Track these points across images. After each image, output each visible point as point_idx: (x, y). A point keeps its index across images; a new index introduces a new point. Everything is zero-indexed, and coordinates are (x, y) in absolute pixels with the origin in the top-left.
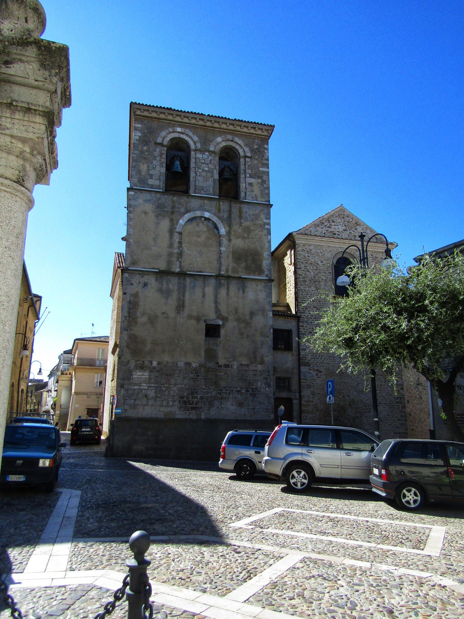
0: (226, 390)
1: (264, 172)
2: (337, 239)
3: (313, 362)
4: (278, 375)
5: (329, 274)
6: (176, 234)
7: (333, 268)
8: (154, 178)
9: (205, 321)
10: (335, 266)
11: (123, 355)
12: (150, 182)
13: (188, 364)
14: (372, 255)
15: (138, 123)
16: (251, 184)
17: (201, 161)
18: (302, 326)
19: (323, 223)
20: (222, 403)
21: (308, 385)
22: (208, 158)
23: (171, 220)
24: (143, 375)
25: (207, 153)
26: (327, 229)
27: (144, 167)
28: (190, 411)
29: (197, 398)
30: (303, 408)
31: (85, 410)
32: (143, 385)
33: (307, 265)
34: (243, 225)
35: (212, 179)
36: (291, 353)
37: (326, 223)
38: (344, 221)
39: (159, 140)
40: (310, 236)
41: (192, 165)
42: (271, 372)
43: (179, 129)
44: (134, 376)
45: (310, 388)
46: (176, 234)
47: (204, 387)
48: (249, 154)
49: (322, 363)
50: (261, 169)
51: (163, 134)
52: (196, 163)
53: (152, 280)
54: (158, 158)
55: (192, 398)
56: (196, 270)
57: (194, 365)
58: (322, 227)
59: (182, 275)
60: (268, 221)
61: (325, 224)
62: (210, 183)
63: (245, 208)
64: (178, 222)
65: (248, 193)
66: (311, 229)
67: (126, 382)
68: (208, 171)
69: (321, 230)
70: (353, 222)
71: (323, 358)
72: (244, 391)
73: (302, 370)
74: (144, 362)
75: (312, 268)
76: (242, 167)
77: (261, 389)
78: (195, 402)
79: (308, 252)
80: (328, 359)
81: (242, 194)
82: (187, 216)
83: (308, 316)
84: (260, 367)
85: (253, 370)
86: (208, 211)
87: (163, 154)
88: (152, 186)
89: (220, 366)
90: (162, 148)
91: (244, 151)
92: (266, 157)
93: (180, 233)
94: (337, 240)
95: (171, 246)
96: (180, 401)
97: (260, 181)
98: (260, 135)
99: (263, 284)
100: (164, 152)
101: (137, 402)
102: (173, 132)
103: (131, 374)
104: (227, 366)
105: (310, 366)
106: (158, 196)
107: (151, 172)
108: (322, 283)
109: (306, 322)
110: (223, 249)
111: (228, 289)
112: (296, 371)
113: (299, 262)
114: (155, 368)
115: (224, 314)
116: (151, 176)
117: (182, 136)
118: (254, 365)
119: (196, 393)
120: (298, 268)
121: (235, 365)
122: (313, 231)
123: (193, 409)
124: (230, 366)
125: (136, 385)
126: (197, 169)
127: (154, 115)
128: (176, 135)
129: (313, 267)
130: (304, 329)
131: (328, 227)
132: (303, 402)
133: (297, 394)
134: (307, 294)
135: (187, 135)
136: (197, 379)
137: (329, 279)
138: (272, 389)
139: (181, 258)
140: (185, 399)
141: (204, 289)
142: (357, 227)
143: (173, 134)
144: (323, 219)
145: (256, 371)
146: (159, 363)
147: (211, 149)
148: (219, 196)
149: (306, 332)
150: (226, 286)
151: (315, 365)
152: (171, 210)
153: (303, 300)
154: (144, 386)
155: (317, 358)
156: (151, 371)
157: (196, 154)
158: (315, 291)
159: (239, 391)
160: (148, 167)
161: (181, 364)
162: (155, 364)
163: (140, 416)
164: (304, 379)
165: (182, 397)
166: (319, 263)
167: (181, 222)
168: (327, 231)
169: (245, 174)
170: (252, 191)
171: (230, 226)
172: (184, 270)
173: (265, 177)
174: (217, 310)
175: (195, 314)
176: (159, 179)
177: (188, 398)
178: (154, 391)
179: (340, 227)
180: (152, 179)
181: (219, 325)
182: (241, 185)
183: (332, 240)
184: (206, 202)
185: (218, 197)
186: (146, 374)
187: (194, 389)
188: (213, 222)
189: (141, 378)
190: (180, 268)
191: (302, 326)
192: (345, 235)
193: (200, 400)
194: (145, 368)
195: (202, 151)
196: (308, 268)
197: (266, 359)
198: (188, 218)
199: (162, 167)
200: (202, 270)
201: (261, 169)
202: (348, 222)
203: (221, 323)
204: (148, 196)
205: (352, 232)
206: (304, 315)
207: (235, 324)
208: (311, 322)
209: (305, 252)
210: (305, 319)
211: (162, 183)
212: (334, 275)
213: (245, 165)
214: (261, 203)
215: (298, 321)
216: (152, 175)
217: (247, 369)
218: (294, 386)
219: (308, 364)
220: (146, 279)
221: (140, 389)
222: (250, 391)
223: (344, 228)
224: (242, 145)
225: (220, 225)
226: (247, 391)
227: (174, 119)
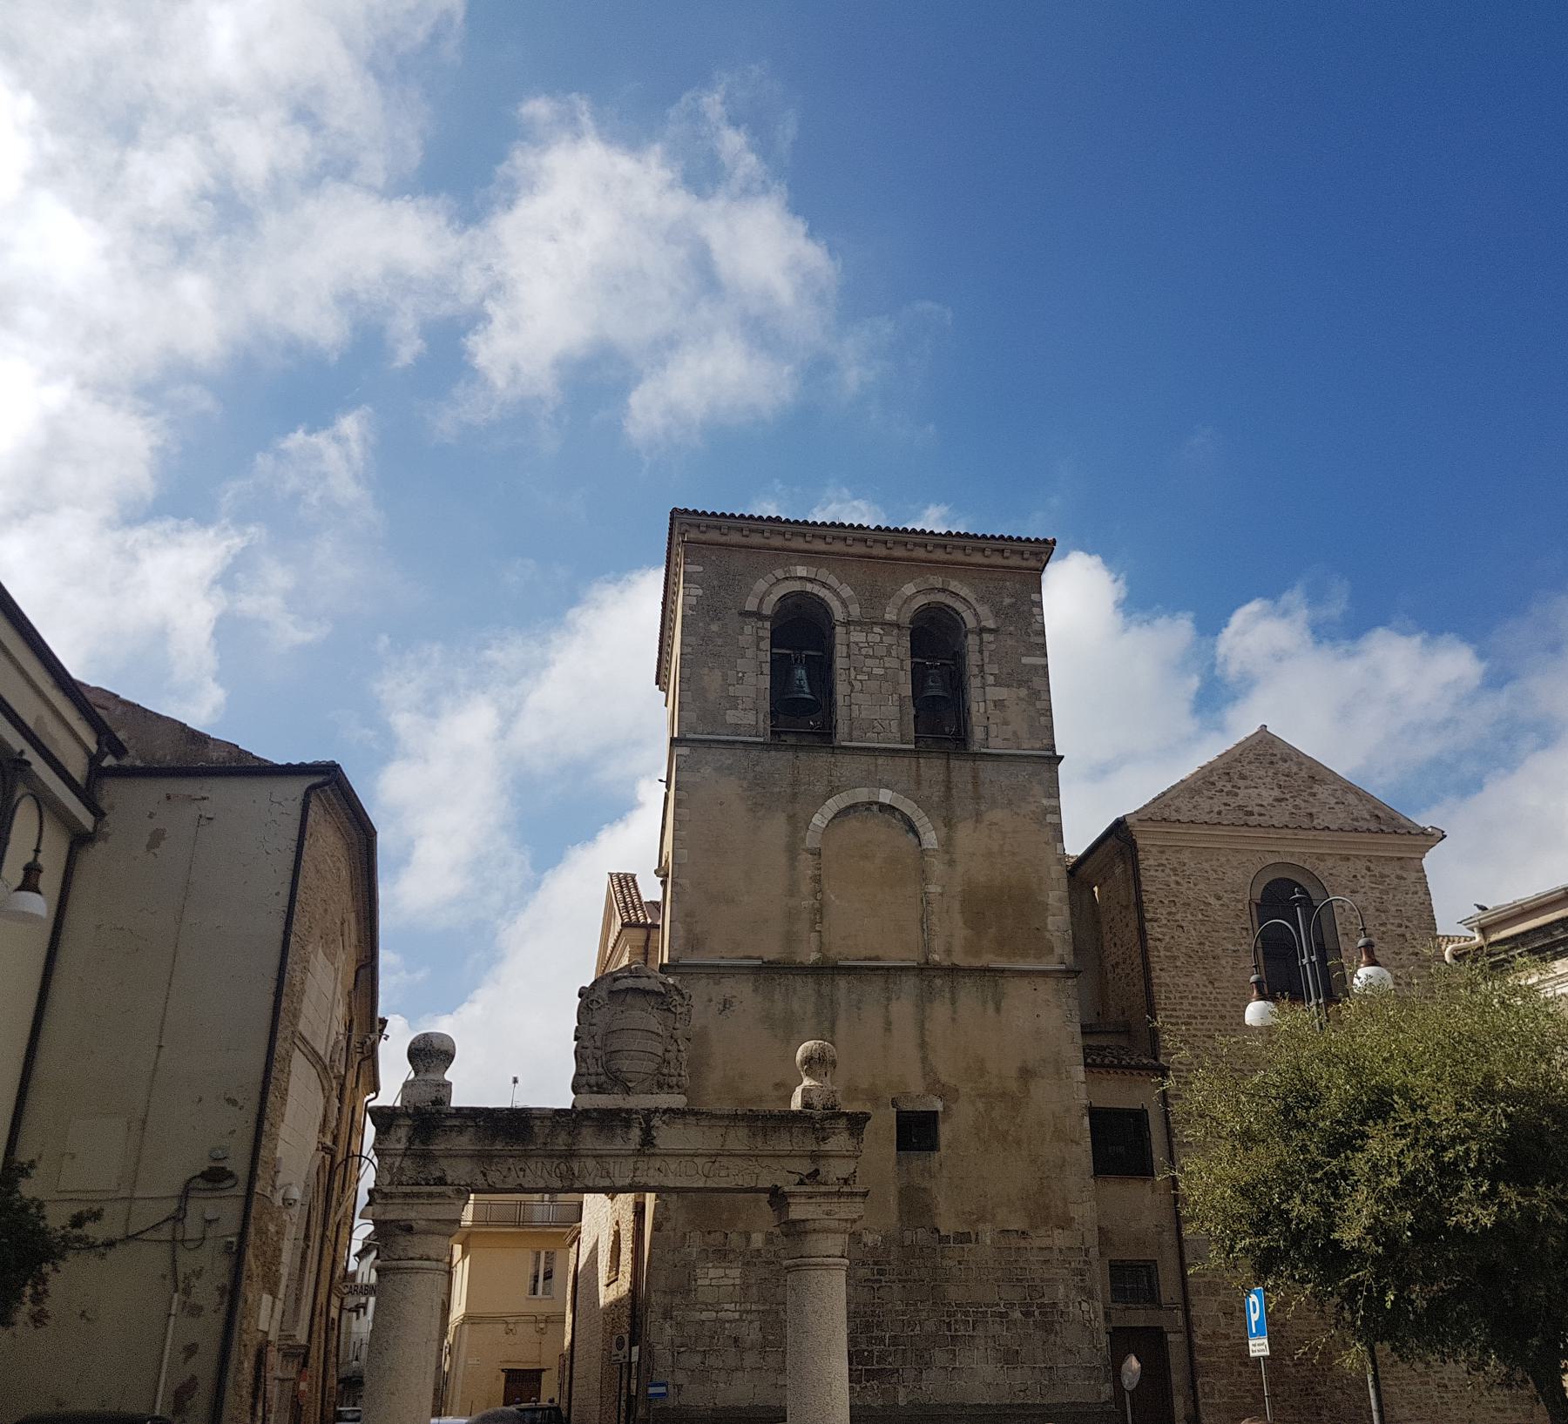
0: (966, 1314)
1: (1035, 668)
2: (1259, 829)
5: (1245, 933)
6: (804, 856)
7: (1254, 913)
8: (740, 707)
9: (894, 1103)
11: (668, 1219)
12: (731, 717)
16: (999, 704)
17: (864, 651)
19: (1213, 784)
23: (792, 818)
25: (877, 629)
27: (712, 680)
29: (882, 1340)
31: (497, 1378)
32: (726, 1306)
33: (1174, 910)
36: (1149, 1184)
37: (1222, 783)
39: (751, 605)
40: (1178, 825)
41: (840, 663)
42: (1094, 1252)
43: (801, 571)
45: (1216, 1293)
46: (804, 856)
48: (990, 624)
50: (1025, 660)
51: (761, 585)
52: (849, 656)
54: (750, 653)
55: (869, 1343)
56: (864, 953)
57: (869, 1239)
58: (1210, 794)
59: (826, 970)
60: (1053, 802)
61: (1219, 785)
62: (891, 709)
63: (988, 770)
66: (1177, 802)
67: (677, 1300)
68: (884, 678)
69: (1206, 806)
70: (1303, 774)
75: (1190, 917)
76: (973, 659)
79: (1174, 870)
81: (978, 733)
82: (834, 804)
84: (1060, 1239)
87: (762, 638)
91: (976, 614)
92: (1037, 627)
93: (817, 853)
94: (1260, 833)
95: (792, 891)
97: (1023, 692)
98: (1016, 568)
99: (1051, 983)
101: (712, 1361)
102: (787, 578)
104: (963, 1238)
108: (1223, 962)
110: (934, 889)
111: (953, 1002)
112: (1168, 1238)
116: (733, 702)
117: (809, 587)
118: (1042, 1232)
119: (879, 1324)
120: (1151, 920)
122: (1184, 809)
124: (973, 1237)
125: (707, 1306)
127: (735, 538)
128: (796, 586)
129: (1192, 914)
131: (1228, 793)
132: (1198, 1341)
133: (1180, 1313)
134: (1181, 998)
135: (824, 585)
137: (1245, 947)
138: (1099, 1306)
141: (886, 1007)
142: (1316, 788)
144: (1211, 771)
147: (887, 617)
150: (948, 995)
152: (789, 790)
153: (1171, 1016)
154: (730, 1311)
157: (848, 633)
158: (1205, 986)
159: (1001, 1315)
160: (725, 677)
166: (1212, 900)
167: (818, 820)
168: (1226, 804)
171: (949, 823)
172: (832, 954)
173: (1037, 682)
174: (928, 1071)
175: (864, 1084)
178: (757, 1324)
179: (1264, 793)
182: (974, 707)
183: (1244, 831)
185: (913, 747)
188: (903, 814)
189: (718, 1287)
190: (820, 951)
192: (1280, 816)
194: (731, 1256)
195: (865, 624)
196: (1178, 917)
197: (1076, 1212)
198: (835, 810)
200: (880, 953)
201: (1025, 660)
202: (1288, 776)
203: (938, 1106)
204: (726, 757)
205: (1303, 805)
209: (1168, 871)
210: (1185, 1074)
211: (761, 717)
213: (981, 652)
214: (1032, 756)
217: (1023, 1244)
218: (1168, 1290)
220: (729, 987)
221: (716, 1320)
222: (1036, 1313)
223: (1276, 793)
224: (971, 598)
226: (1027, 1314)
227: (787, 543)
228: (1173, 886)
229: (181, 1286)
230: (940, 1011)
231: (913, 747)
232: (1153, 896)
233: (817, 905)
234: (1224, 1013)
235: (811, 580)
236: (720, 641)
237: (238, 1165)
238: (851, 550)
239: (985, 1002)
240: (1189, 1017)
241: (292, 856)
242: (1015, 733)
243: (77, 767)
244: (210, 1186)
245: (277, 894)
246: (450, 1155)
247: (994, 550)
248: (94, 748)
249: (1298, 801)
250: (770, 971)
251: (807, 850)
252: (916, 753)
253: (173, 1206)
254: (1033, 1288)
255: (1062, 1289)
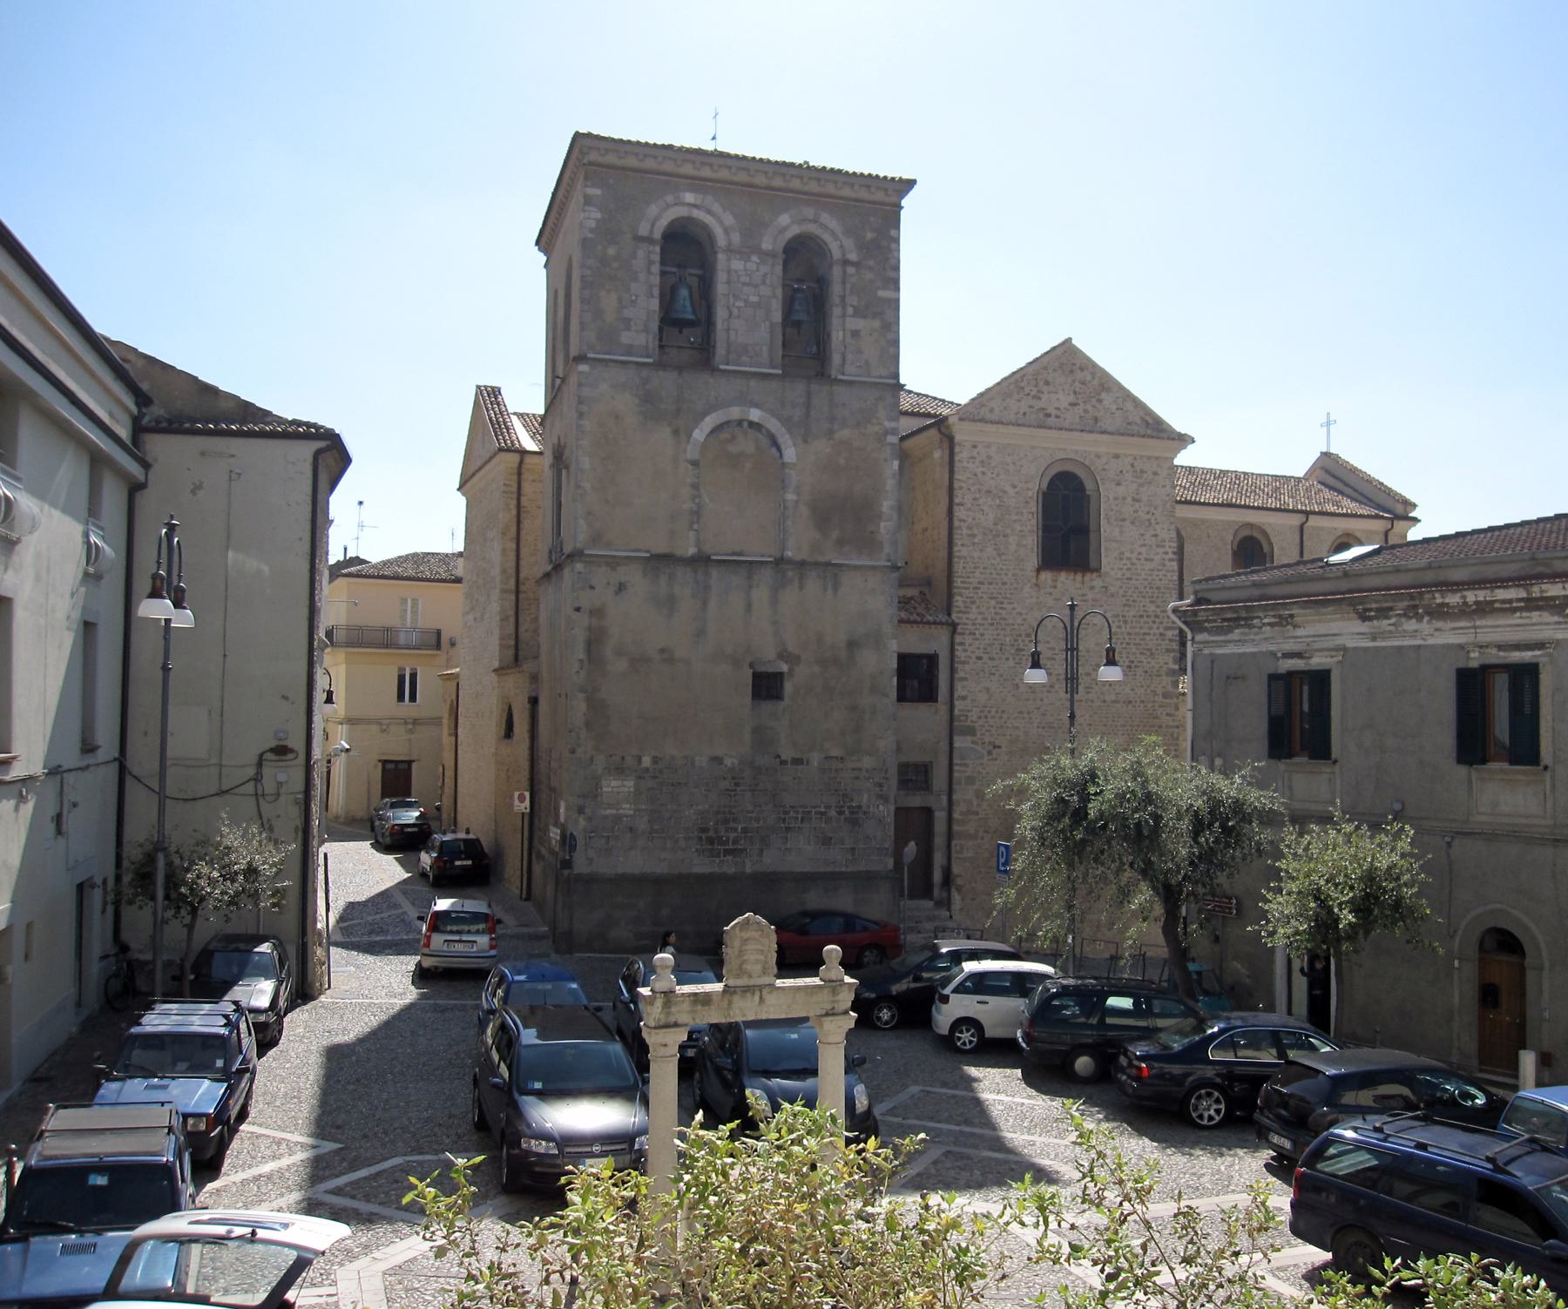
0: (797, 812)
3: (983, 726)
4: (904, 759)
7: (1040, 500)
8: (633, 329)
9: (751, 665)
10: (1044, 493)
12: (626, 338)
13: (717, 760)
14: (1132, 465)
15: (593, 186)
17: (743, 279)
18: (962, 644)
19: (1023, 388)
20: (786, 838)
21: (969, 777)
22: (758, 270)
24: (624, 786)
25: (755, 258)
26: (1033, 402)
28: (722, 858)
29: (736, 830)
30: (956, 828)
31: (376, 766)
32: (624, 806)
33: (978, 496)
34: (837, 436)
35: (767, 323)
38: (1074, 381)
39: (643, 230)
43: (689, 197)
44: (604, 789)
47: (750, 808)
48: (853, 257)
49: (1002, 727)
51: (653, 210)
53: (634, 577)
55: (726, 831)
57: (728, 762)
59: (701, 561)
61: (1027, 390)
62: (763, 333)
64: (689, 436)
65: (849, 357)
71: (1005, 716)
72: (833, 813)
73: (957, 744)
74: (623, 758)
76: (836, 289)
77: (868, 807)
78: (731, 839)
80: (1015, 718)
81: (836, 359)
82: (709, 422)
83: (976, 619)
85: (853, 769)
86: (757, 406)
88: (629, 350)
89: (783, 763)
90: (651, 248)
92: (892, 262)
96: (700, 838)
97: (877, 324)
100: (656, 258)
102: (676, 204)
103: (598, 786)
104: (797, 761)
105: (975, 735)
106: (645, 372)
107: (627, 313)
109: (970, 634)
110: (790, 497)
111: (801, 588)
112: (944, 746)
113: (961, 488)
114: (647, 770)
115: (792, 647)
117: (696, 213)
120: (958, 505)
121: (815, 759)
123: (727, 852)
126: (732, 300)
128: (681, 212)
130: (966, 651)
131: (1034, 397)
132: (956, 815)
135: (709, 212)
136: (735, 790)
139: (698, 522)
140: (711, 833)
142: (1104, 395)
143: (676, 208)
145: (860, 769)
146: (655, 760)
148: (783, 367)
149: (970, 657)
151: (987, 733)
153: (965, 582)
154: (627, 809)
155: (993, 717)
156: (640, 777)
157: (729, 260)
159: (822, 814)
160: (620, 300)
161: (702, 761)
162: (647, 761)
163: (620, 871)
164: (961, 765)
165: (704, 830)
167: (699, 435)
168: (1031, 407)
169: (844, 308)
170: (860, 351)
172: (707, 549)
176: (646, 330)
177: (716, 831)
180: (629, 330)
181: (781, 675)
182: (834, 335)
184: (753, 383)
185: (780, 372)
186: (630, 784)
187: (730, 812)
188: (768, 431)
189: (618, 793)
191: (962, 644)
193: (743, 835)
195: (744, 254)
199: (652, 296)
203: (785, 668)
206: (967, 619)
207: (817, 669)
208: (982, 635)
210: (969, 627)
211: (651, 337)
212: (1040, 518)
213: (844, 283)
215: (954, 632)
216: (629, 320)
217: (841, 766)
218: (939, 779)
219: (971, 731)
222: (847, 812)
225: (785, 439)
226: (840, 813)
228: (980, 475)
229: (266, 826)
230: (790, 596)
231: (780, 372)
232: (963, 485)
233: (695, 509)
234: (1005, 579)
235: (695, 206)
236: (615, 265)
237: (297, 743)
238: (736, 179)
239: (825, 590)
240: (979, 583)
241: (309, 509)
242: (867, 362)
243: (124, 433)
244: (277, 758)
245: (301, 539)
246: (679, 1012)
247: (861, 185)
248: (134, 409)
249: (1089, 407)
250: (660, 562)
251: (687, 461)
252: (783, 377)
253: (251, 772)
254: (845, 795)
255: (866, 796)
